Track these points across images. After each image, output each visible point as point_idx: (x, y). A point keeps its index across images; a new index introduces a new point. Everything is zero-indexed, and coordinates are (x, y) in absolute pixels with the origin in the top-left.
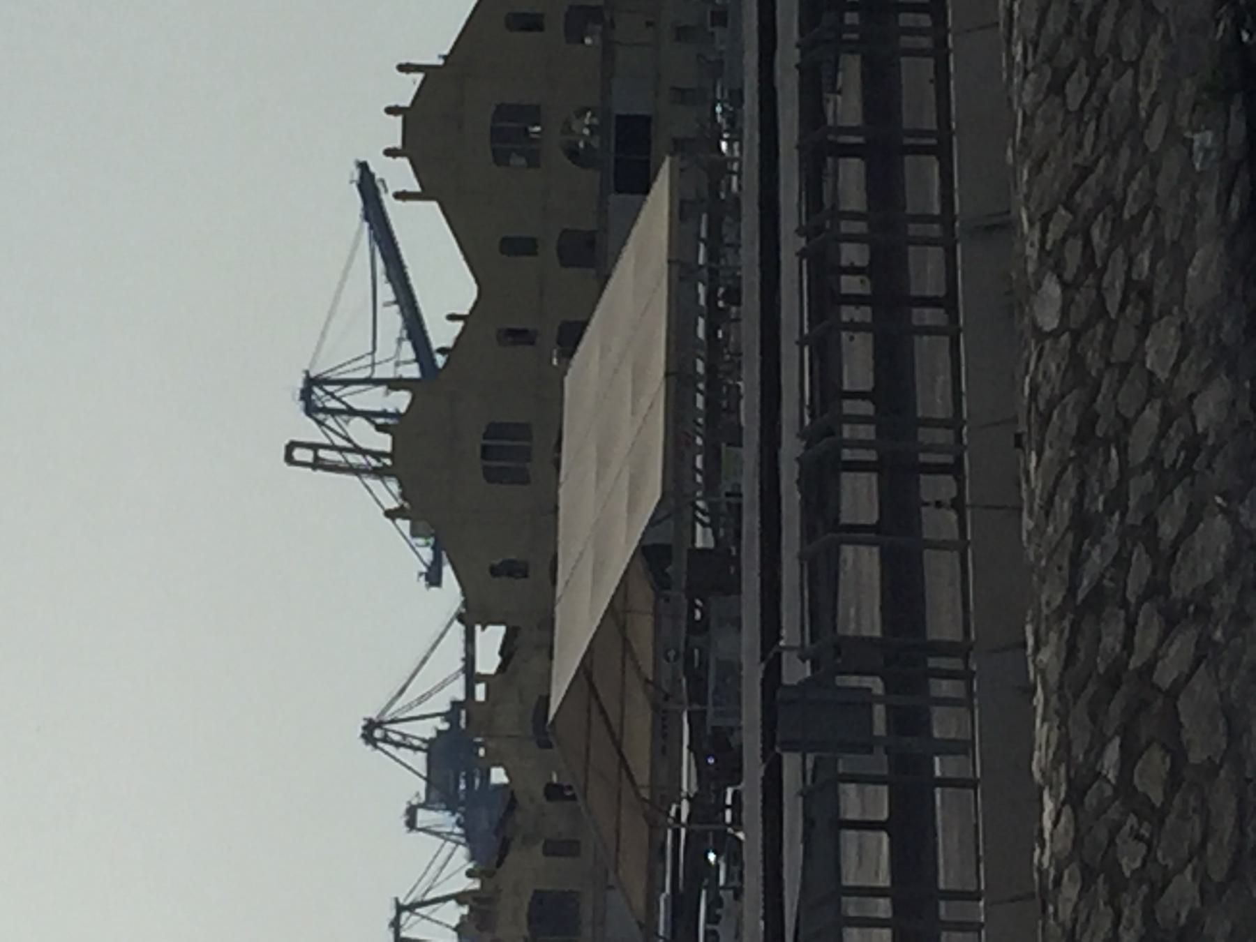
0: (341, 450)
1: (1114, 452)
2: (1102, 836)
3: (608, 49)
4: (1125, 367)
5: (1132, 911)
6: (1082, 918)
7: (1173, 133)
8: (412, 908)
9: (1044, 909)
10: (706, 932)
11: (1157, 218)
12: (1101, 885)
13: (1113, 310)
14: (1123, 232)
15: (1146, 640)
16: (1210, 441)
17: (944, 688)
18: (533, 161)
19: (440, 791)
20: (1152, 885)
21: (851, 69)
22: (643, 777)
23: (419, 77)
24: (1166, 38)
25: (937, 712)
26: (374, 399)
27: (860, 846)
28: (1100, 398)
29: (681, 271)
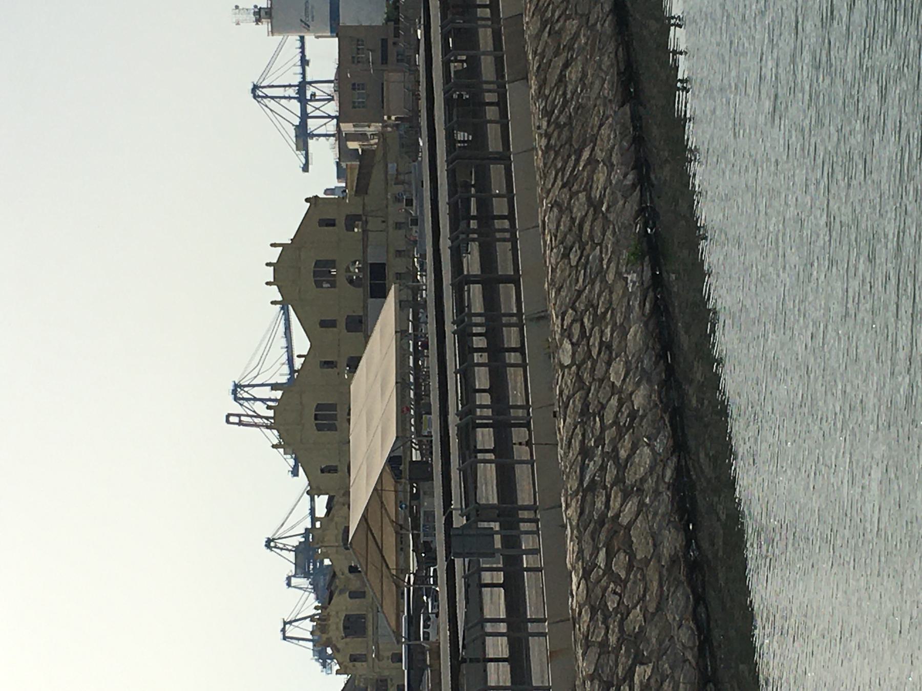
0: (251, 416)
1: (597, 419)
2: (598, 591)
3: (365, 231)
4: (601, 381)
5: (614, 626)
6: (591, 630)
7: (618, 274)
8: (290, 623)
9: (575, 626)
10: (424, 632)
11: (612, 313)
12: (599, 615)
13: (595, 355)
14: (598, 320)
15: (615, 504)
16: (641, 413)
17: (524, 526)
18: (333, 285)
19: (301, 569)
20: (622, 614)
21: (474, 247)
22: (392, 565)
23: (281, 248)
24: (614, 233)
25: (523, 537)
26: (266, 393)
27: (492, 595)
28: (590, 395)
29: (401, 333)
